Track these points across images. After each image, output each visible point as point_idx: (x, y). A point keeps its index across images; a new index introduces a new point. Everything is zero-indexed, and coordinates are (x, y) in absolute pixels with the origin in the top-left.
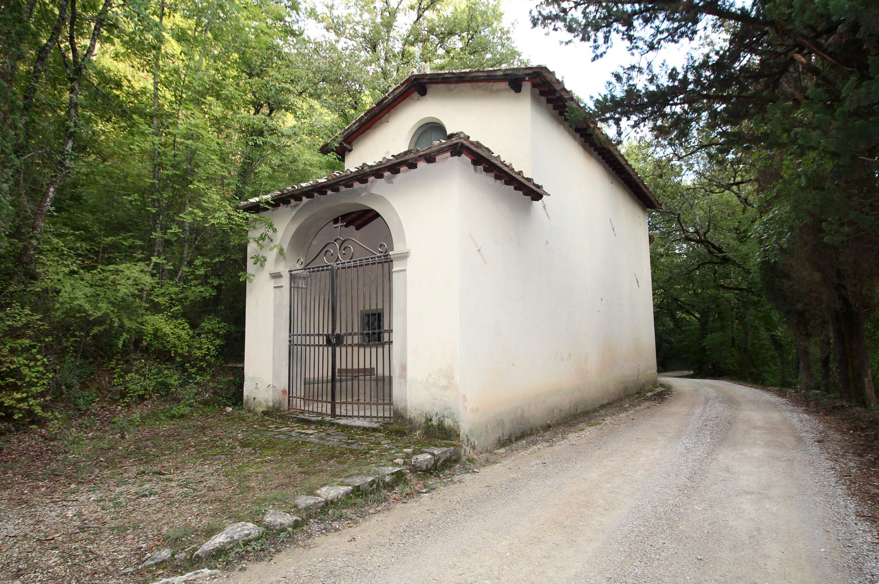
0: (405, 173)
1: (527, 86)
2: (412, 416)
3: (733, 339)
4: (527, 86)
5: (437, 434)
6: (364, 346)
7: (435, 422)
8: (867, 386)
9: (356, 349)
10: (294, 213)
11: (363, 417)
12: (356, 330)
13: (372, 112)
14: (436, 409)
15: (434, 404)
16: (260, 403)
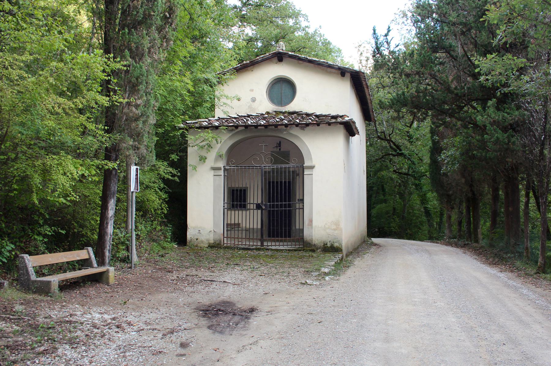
2: (316, 243)
3: (394, 209)
4: (348, 75)
7: (329, 245)
8: (479, 233)
10: (231, 134)
16: (202, 242)
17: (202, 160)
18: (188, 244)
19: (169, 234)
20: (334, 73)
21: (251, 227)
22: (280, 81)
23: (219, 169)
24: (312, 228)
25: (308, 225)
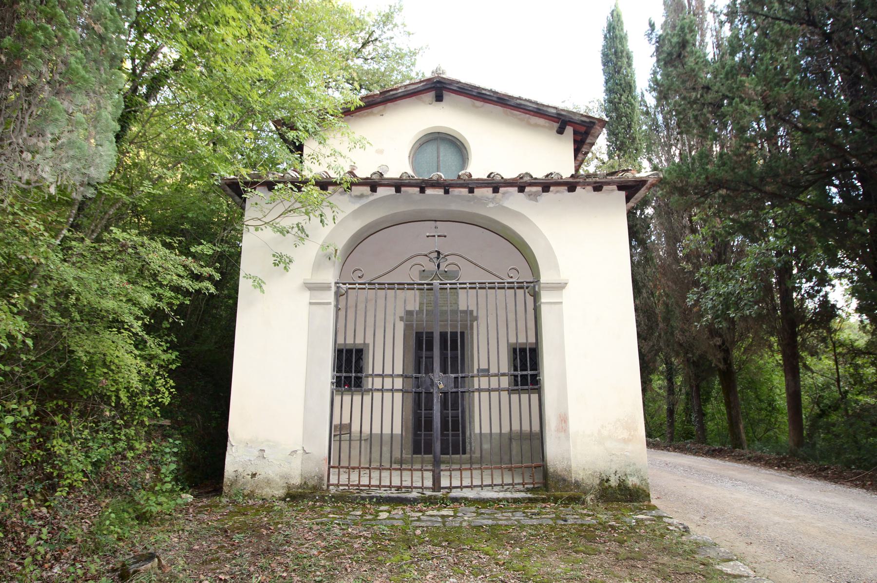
0: (558, 195)
1: (569, 130)
4: (569, 130)
5: (619, 496)
6: (518, 392)
7: (614, 482)
9: (504, 394)
10: (357, 206)
11: (490, 486)
12: (399, 370)
13: (370, 99)
14: (614, 467)
15: (612, 460)
16: (268, 482)
17: (282, 265)
18: (226, 489)
19: (170, 466)
20: (544, 127)
21: (366, 429)
22: (435, 139)
23: (325, 287)
24: (567, 437)
25: (558, 430)
